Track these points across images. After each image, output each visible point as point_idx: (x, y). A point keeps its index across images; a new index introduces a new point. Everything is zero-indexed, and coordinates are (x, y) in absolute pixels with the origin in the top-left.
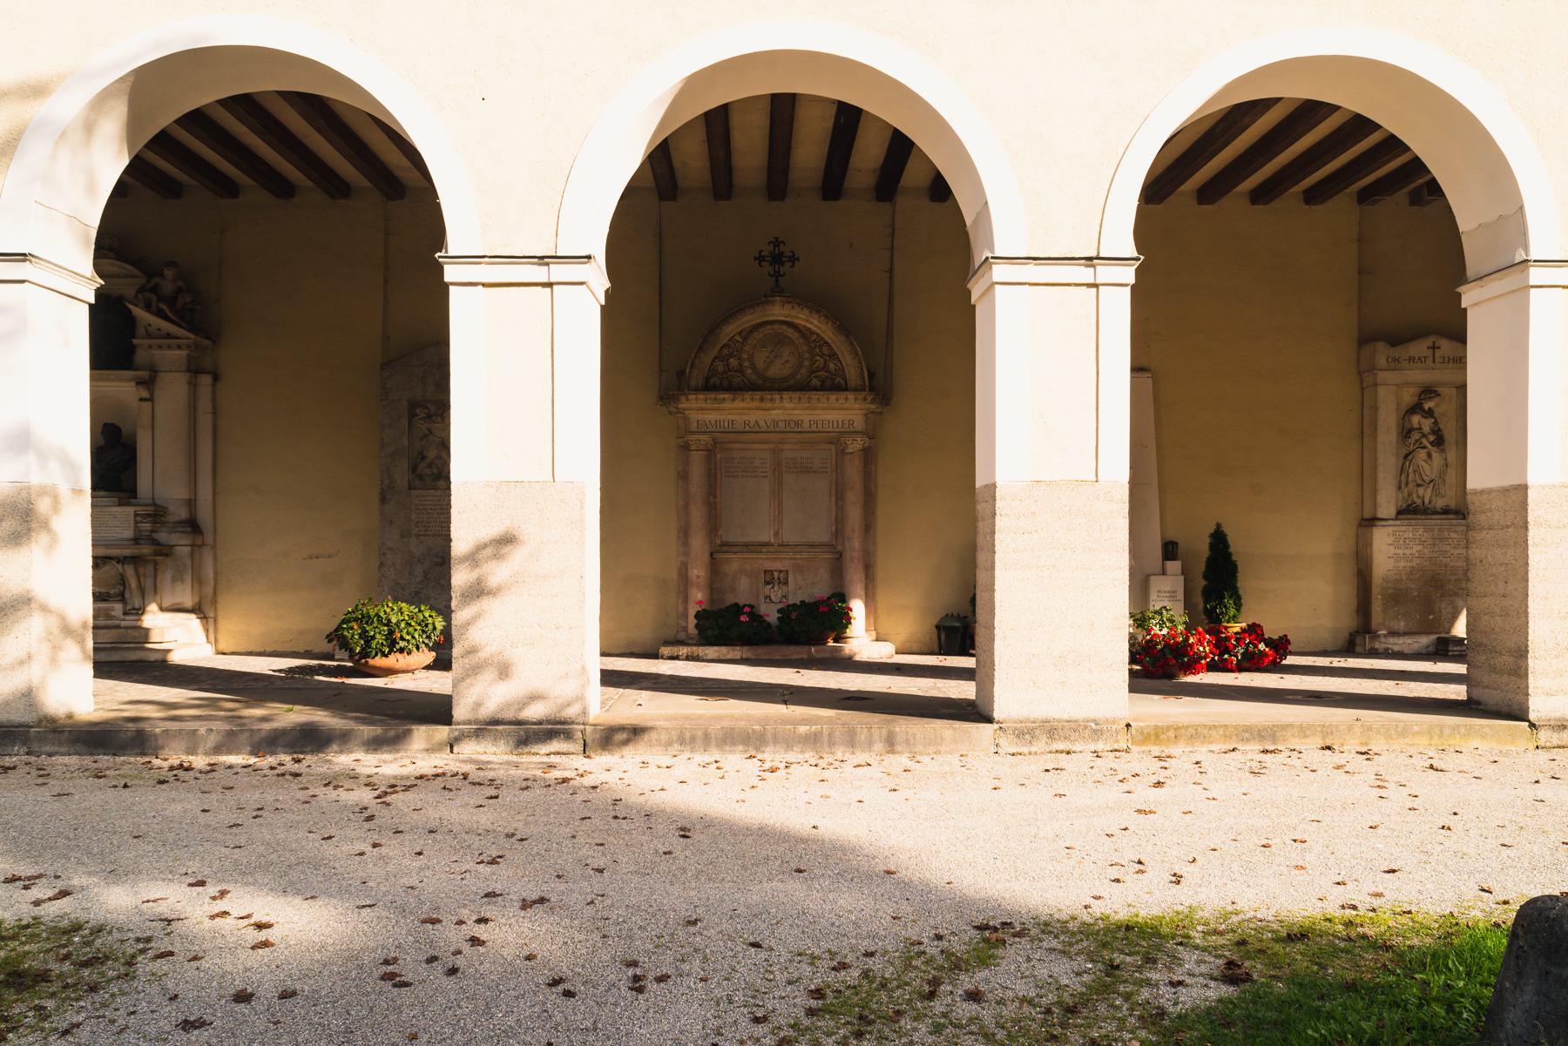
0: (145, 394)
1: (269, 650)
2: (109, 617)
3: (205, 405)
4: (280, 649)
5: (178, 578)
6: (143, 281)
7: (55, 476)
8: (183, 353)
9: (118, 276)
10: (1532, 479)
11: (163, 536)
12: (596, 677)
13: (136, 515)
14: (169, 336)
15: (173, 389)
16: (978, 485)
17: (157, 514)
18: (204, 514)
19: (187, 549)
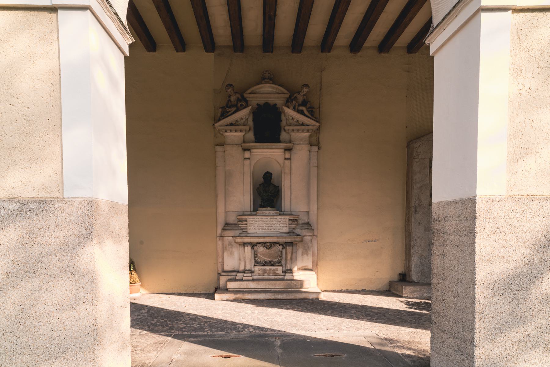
0: (287, 156)
1: (344, 289)
2: (276, 274)
3: (314, 162)
4: (349, 288)
5: (305, 252)
6: (287, 96)
7: (103, 195)
8: (307, 134)
9: (273, 93)
10: (483, 190)
11: (298, 231)
12: (125, 318)
13: (289, 220)
14: (302, 124)
15: (301, 153)
16: (435, 199)
17: (295, 220)
18: (313, 219)
19: (309, 238)
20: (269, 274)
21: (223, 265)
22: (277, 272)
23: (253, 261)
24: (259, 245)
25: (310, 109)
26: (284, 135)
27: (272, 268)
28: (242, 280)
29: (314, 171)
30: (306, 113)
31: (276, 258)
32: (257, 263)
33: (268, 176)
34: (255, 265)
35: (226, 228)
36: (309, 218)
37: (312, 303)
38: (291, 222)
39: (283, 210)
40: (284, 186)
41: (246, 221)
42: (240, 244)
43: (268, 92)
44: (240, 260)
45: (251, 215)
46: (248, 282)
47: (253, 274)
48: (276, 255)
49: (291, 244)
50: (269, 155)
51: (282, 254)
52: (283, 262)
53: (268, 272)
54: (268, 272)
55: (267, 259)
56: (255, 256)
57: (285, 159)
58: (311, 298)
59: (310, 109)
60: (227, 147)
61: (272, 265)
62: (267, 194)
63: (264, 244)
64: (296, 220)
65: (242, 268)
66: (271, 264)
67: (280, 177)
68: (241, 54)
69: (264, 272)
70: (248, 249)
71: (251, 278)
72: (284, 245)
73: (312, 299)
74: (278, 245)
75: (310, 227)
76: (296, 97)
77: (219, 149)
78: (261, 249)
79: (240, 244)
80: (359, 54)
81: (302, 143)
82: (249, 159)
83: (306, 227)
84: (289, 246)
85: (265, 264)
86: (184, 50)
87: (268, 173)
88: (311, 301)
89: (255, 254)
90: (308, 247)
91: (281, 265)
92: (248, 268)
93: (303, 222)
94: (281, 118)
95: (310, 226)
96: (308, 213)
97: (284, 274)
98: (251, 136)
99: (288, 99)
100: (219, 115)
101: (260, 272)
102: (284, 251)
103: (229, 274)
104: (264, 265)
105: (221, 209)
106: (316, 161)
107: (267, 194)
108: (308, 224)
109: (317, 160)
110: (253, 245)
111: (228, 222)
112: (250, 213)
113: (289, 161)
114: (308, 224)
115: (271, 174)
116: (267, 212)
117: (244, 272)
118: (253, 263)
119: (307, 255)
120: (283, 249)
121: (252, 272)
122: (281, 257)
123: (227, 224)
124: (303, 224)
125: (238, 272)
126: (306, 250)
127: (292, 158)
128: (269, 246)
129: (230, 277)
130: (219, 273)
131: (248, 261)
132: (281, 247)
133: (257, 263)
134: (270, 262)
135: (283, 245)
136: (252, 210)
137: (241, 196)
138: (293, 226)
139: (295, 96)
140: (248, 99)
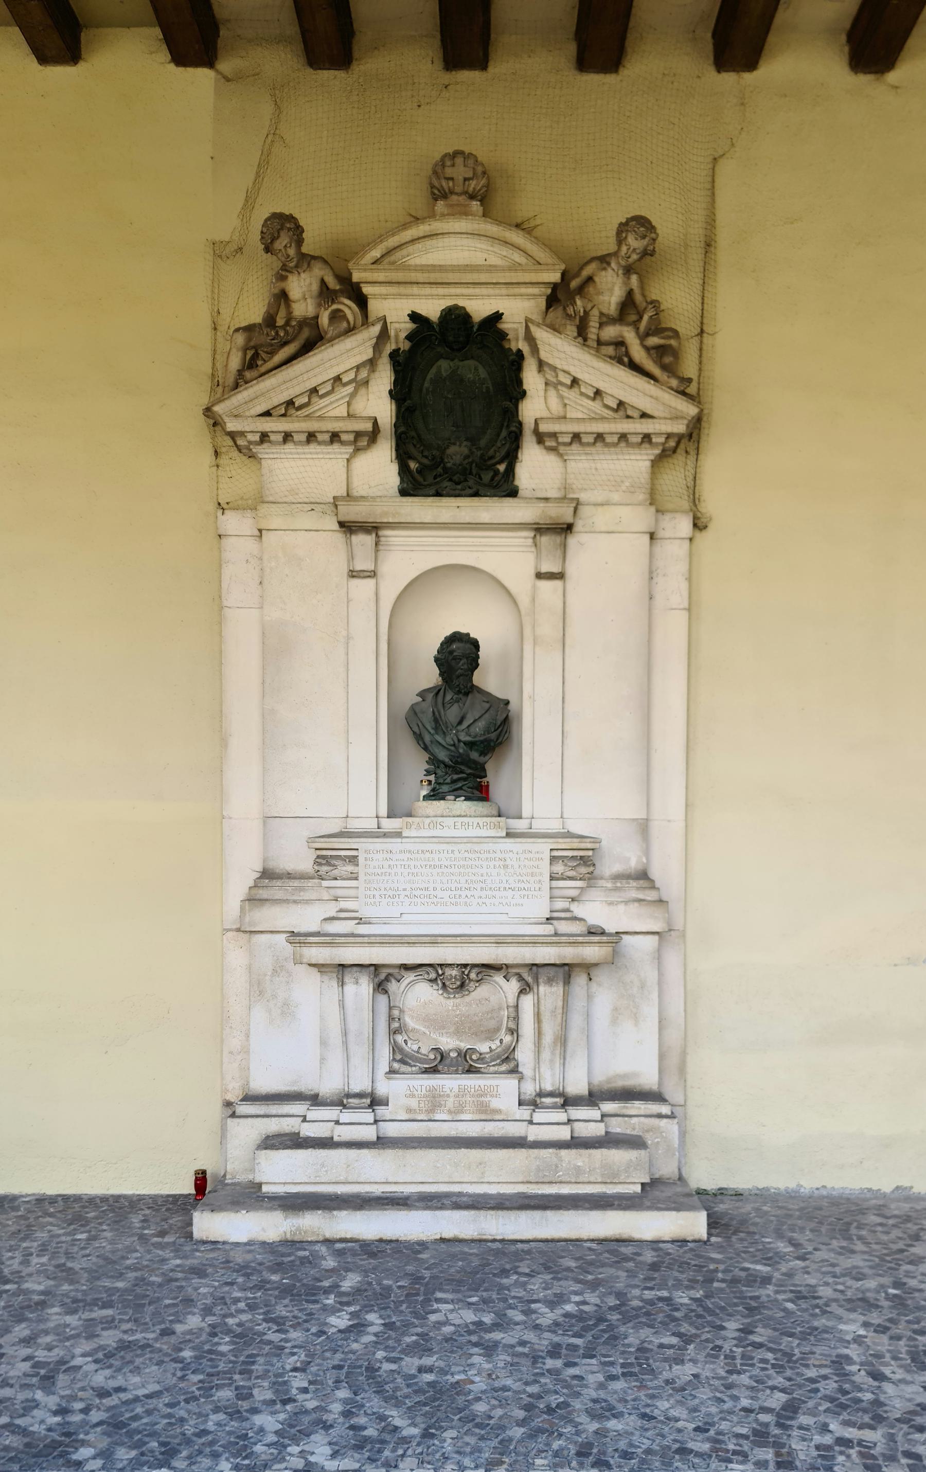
2: (487, 1113)
3: (673, 588)
6: (555, 277)
13: (553, 859)
15: (607, 552)
20: (455, 1117)
21: (245, 1069)
22: (495, 1103)
23: (384, 1053)
24: (410, 977)
25: (653, 341)
26: (534, 467)
27: (471, 1082)
28: (326, 1143)
29: (672, 630)
30: (638, 354)
31: (491, 1034)
32: (402, 1059)
33: (459, 657)
34: (392, 1071)
35: (263, 894)
36: (647, 852)
37: (654, 1267)
38: (559, 868)
39: (526, 812)
40: (532, 698)
41: (353, 860)
42: (321, 967)
43: (464, 267)
44: (324, 1043)
45: (380, 834)
46: (353, 1153)
47: (381, 1111)
48: (492, 1024)
49: (566, 972)
50: (466, 563)
51: (517, 1018)
52: (524, 1055)
53: (450, 1103)
54: (450, 1103)
55: (448, 1043)
56: (396, 1028)
57: (539, 576)
58: (648, 1235)
59: (653, 341)
60: (274, 519)
61: (471, 1070)
62: (459, 736)
63: (435, 973)
64: (585, 861)
65: (329, 1086)
66: (467, 1063)
67: (514, 663)
68: (340, 74)
69: (435, 1101)
70: (360, 990)
71: (369, 1133)
72: (530, 975)
73: (655, 1244)
74: (499, 978)
75: (651, 895)
76: (590, 279)
77: (232, 522)
78: (418, 996)
79: (321, 967)
80: (892, 77)
81: (616, 497)
82: (373, 574)
83: (634, 894)
84: (550, 981)
85: (440, 1062)
86: (70, 52)
87: (456, 638)
88: (649, 1256)
89: (391, 1019)
90: (643, 986)
91: (514, 1071)
92: (360, 1084)
93: (617, 868)
94: (520, 382)
95: (653, 886)
96: (644, 828)
97: (525, 1113)
98: (379, 468)
99: (555, 287)
100: (235, 362)
101: (413, 1103)
102: (527, 1002)
103: (274, 1109)
104: (434, 1070)
105: (244, 803)
106: (684, 586)
107: (459, 736)
108: (643, 876)
109: (689, 579)
110: (382, 977)
111: (271, 865)
112: (371, 825)
113: (558, 583)
114: (643, 876)
115: (475, 644)
116: (449, 821)
117: (341, 1101)
118: (383, 1066)
119: (636, 1018)
120: (522, 992)
121: (375, 1101)
122: (514, 1032)
123: (267, 875)
124: (617, 877)
125: (315, 1100)
126: (38, 1405)
127: (572, 570)
128: (459, 978)
129: (274, 1126)
130: (228, 1104)
131: (359, 1052)
132: (513, 986)
133: (402, 1059)
134: (464, 1055)
135: (521, 978)
136: (384, 811)
137: (343, 757)
138: (571, 887)
139: (586, 273)
140: (366, 290)
